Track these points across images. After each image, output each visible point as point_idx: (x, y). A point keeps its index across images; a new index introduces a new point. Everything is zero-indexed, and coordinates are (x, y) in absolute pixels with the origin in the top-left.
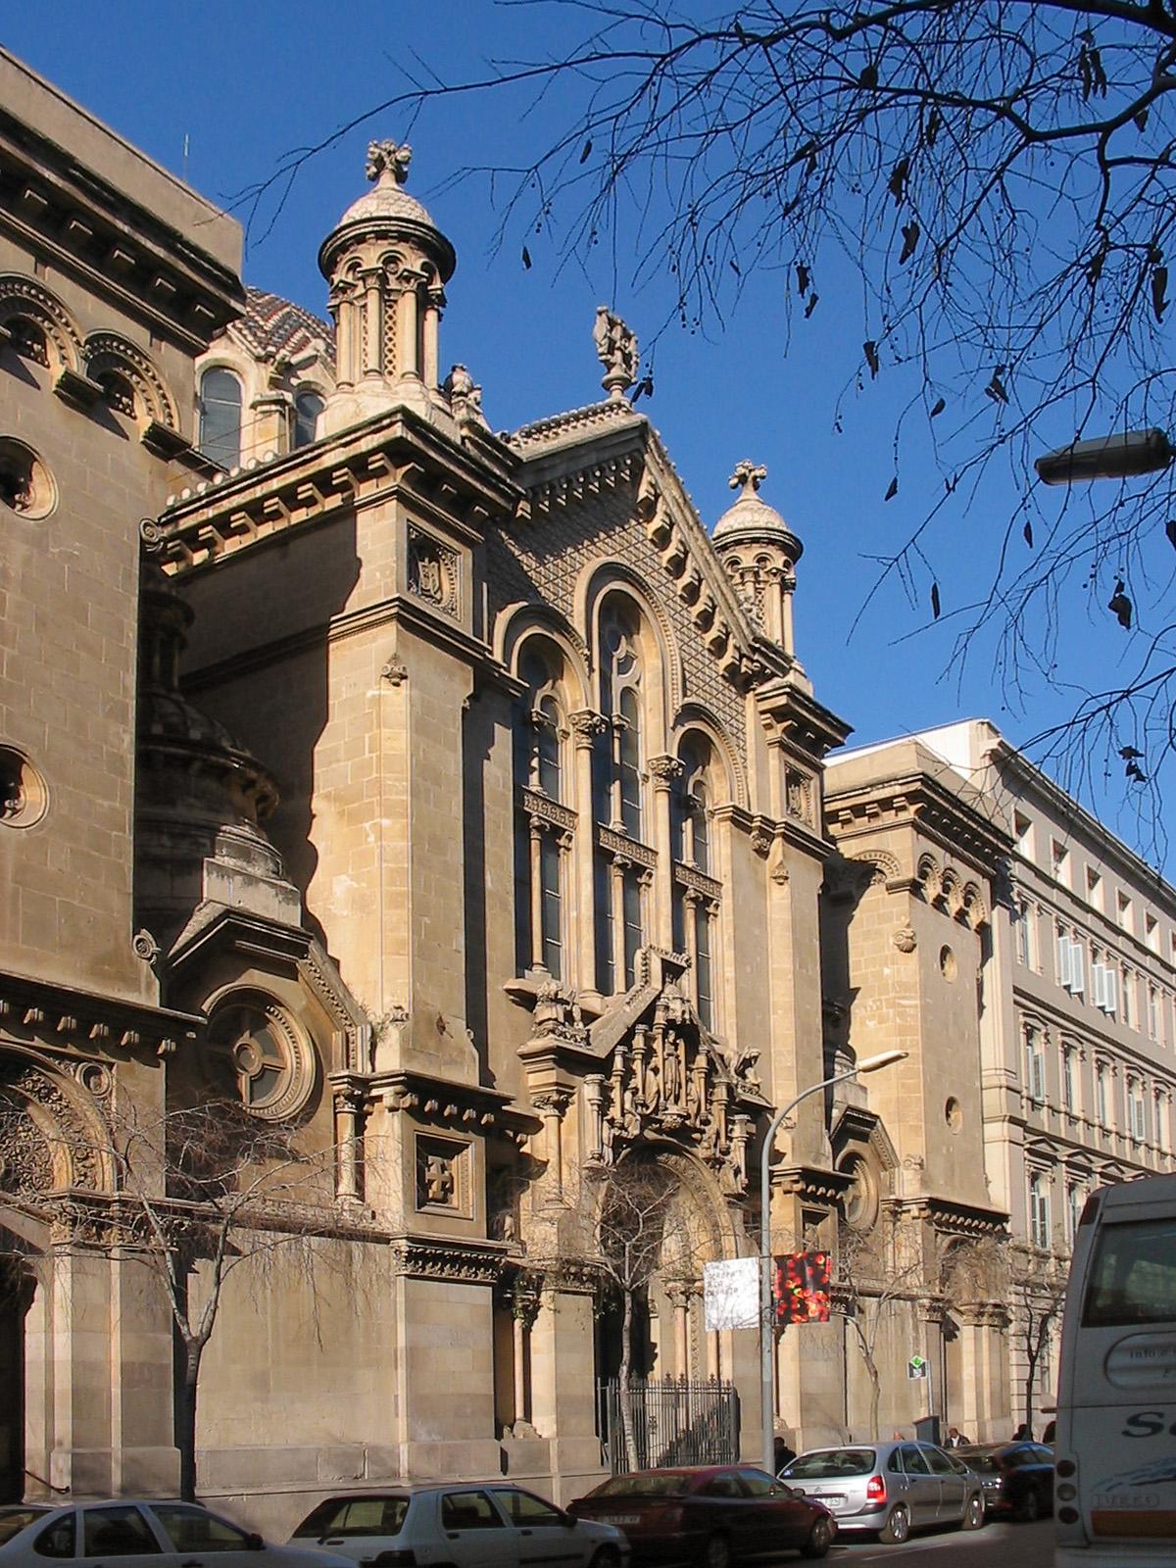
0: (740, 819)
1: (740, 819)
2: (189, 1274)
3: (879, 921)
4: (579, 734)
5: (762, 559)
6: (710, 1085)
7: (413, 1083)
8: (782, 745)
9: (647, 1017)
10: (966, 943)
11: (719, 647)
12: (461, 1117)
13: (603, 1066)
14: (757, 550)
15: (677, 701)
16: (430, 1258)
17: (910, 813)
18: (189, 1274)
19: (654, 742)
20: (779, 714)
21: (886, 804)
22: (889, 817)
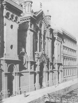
0: (47, 38)
1: (47, 38)
2: (1, 66)
3: (56, 42)
4: (44, 84)
5: (49, 17)
6: (45, 58)
7: (30, 62)
8: (50, 32)
9: (42, 54)
10: (60, 43)
11: (46, 25)
12: (33, 63)
13: (40, 58)
14: (48, 17)
15: (44, 30)
16: (31, 73)
17: (57, 35)
18: (1, 66)
19: (42, 33)
20: (49, 30)
21: (55, 34)
22: (56, 35)
